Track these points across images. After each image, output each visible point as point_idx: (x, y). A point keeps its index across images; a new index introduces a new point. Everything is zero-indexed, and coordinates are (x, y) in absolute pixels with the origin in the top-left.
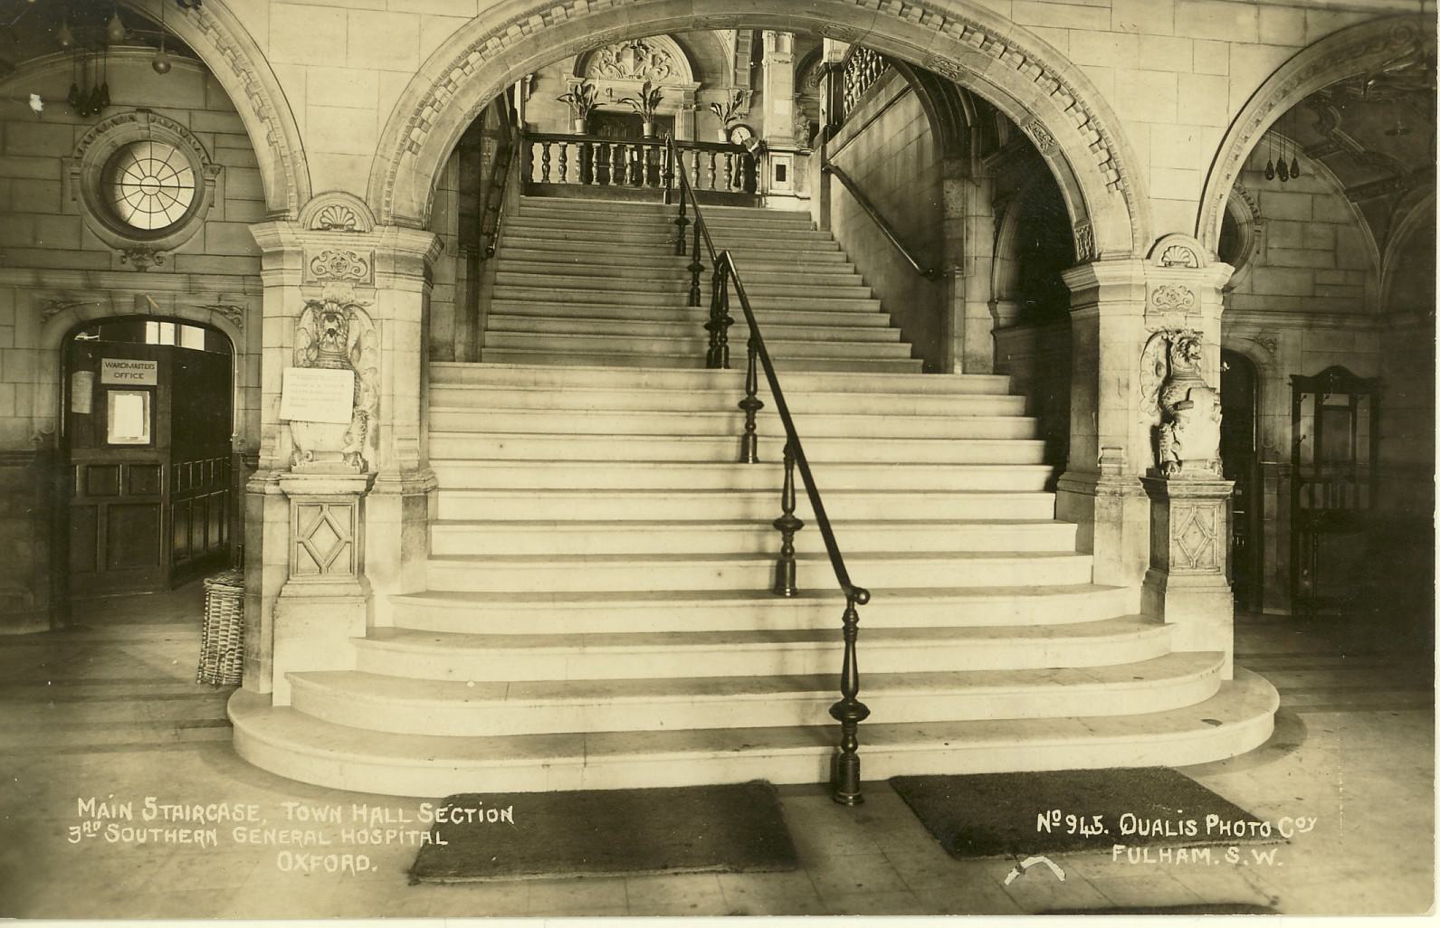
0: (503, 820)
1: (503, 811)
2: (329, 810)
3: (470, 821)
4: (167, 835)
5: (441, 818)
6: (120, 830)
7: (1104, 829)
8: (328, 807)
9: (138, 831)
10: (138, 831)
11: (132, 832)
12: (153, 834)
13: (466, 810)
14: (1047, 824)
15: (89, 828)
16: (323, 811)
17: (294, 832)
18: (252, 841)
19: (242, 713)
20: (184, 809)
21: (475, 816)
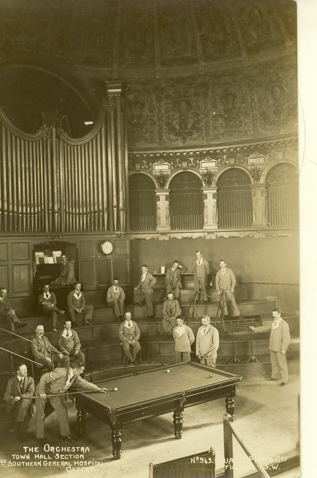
0: (51, 451)
1: (38, 462)
2: (26, 456)
3: (78, 451)
4: (27, 464)
5: (62, 458)
6: (12, 462)
7: (212, 461)
8: (25, 455)
9: (18, 463)
10: (18, 463)
11: (16, 463)
12: (22, 464)
13: (69, 455)
14: (194, 461)
15: (2, 462)
16: (24, 456)
17: (35, 462)
18: (61, 458)
19: (230, 117)
20: (43, 456)
21: (25, 464)
